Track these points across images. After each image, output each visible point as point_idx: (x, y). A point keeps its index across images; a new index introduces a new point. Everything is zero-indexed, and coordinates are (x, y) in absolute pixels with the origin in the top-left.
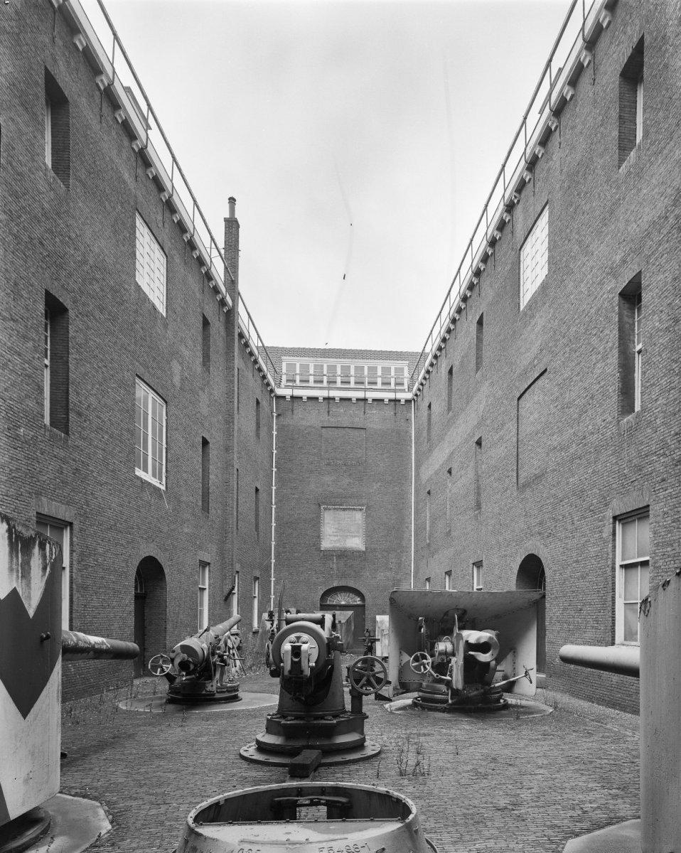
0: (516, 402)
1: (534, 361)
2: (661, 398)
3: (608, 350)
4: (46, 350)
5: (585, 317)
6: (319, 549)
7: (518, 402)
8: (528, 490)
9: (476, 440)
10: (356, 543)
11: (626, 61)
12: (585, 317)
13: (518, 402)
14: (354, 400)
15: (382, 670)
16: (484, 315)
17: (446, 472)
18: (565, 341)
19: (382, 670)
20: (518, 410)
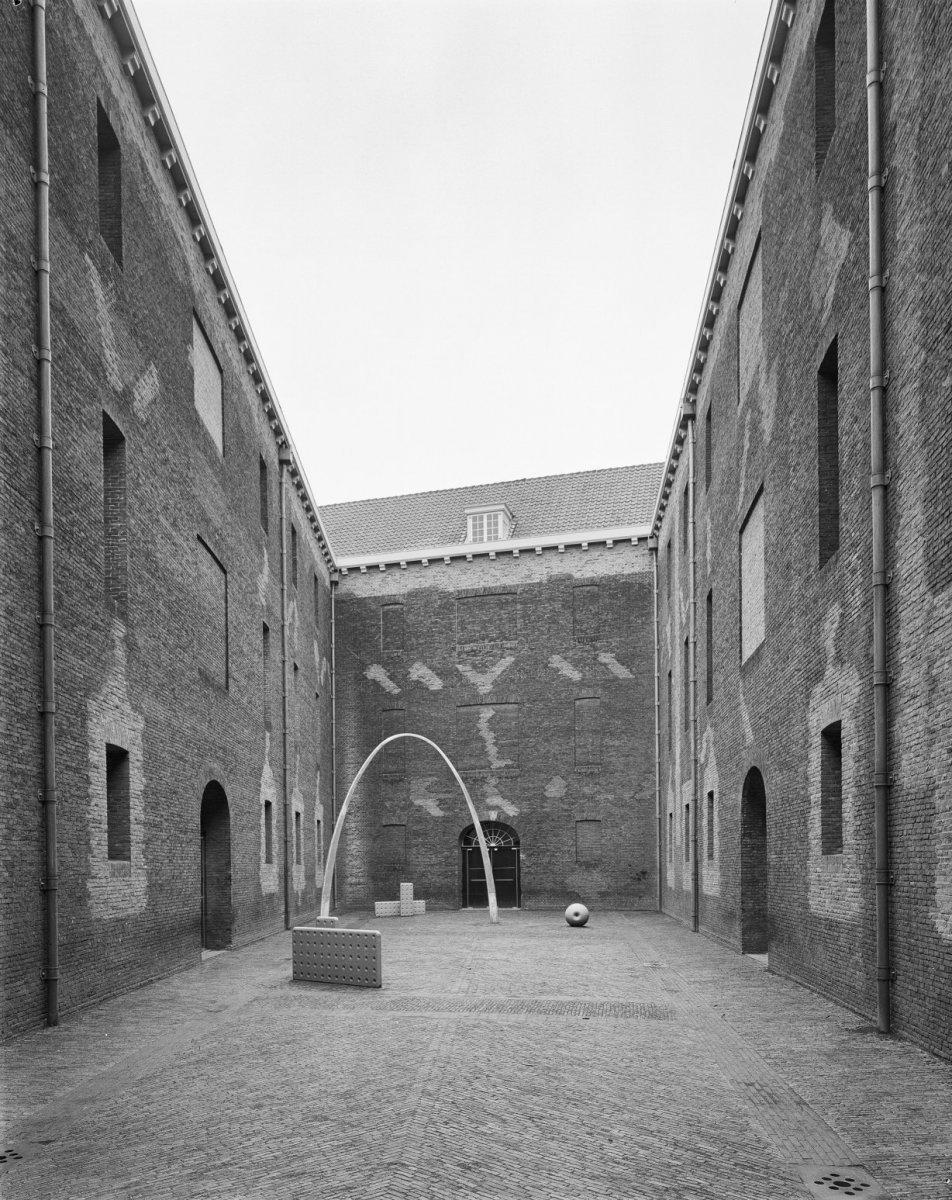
14: (561, 548)
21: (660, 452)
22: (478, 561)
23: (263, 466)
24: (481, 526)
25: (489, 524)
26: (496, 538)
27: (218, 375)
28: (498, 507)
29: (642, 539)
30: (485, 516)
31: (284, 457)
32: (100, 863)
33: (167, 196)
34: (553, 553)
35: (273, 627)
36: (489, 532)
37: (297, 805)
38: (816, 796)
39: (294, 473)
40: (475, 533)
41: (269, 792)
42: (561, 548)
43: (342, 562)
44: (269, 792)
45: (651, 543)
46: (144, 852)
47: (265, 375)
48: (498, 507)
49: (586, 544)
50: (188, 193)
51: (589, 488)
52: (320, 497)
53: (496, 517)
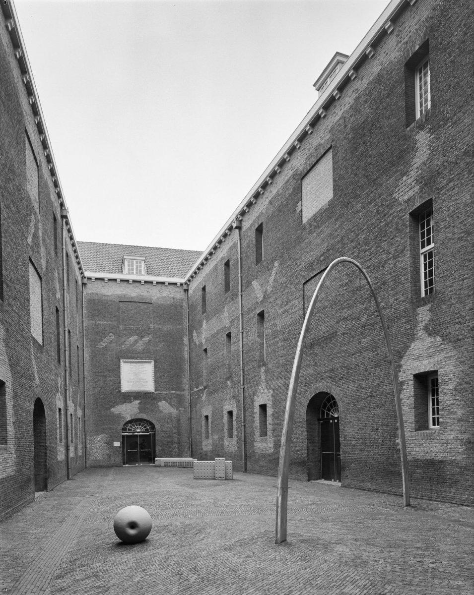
0: (301, 286)
1: (320, 258)
2: (455, 285)
3: (400, 252)
4: (433, 233)
5: (374, 228)
6: (119, 391)
7: (303, 287)
8: (317, 348)
9: (258, 312)
10: (149, 385)
11: (417, 47)
12: (374, 228)
13: (303, 287)
14: (143, 282)
15: (89, 463)
16: (264, 225)
17: (225, 336)
18: (353, 244)
19: (89, 463)
20: (304, 292)
21: (203, 243)
22: (110, 283)
23: (55, 219)
24: (133, 266)
25: (137, 266)
26: (141, 274)
27: (36, 167)
28: (141, 258)
29: (182, 284)
30: (135, 261)
31: (64, 214)
32: (257, 438)
33: (16, 72)
34: (114, 283)
35: (61, 309)
36: (137, 270)
37: (71, 410)
38: (226, 427)
39: (67, 223)
40: (129, 269)
41: (60, 404)
42: (143, 282)
43: (87, 274)
44: (60, 404)
45: (185, 287)
46: (272, 434)
47: (57, 173)
48: (141, 258)
49: (143, 281)
50: (27, 76)
51: (183, 256)
52: (78, 238)
53: (140, 263)
